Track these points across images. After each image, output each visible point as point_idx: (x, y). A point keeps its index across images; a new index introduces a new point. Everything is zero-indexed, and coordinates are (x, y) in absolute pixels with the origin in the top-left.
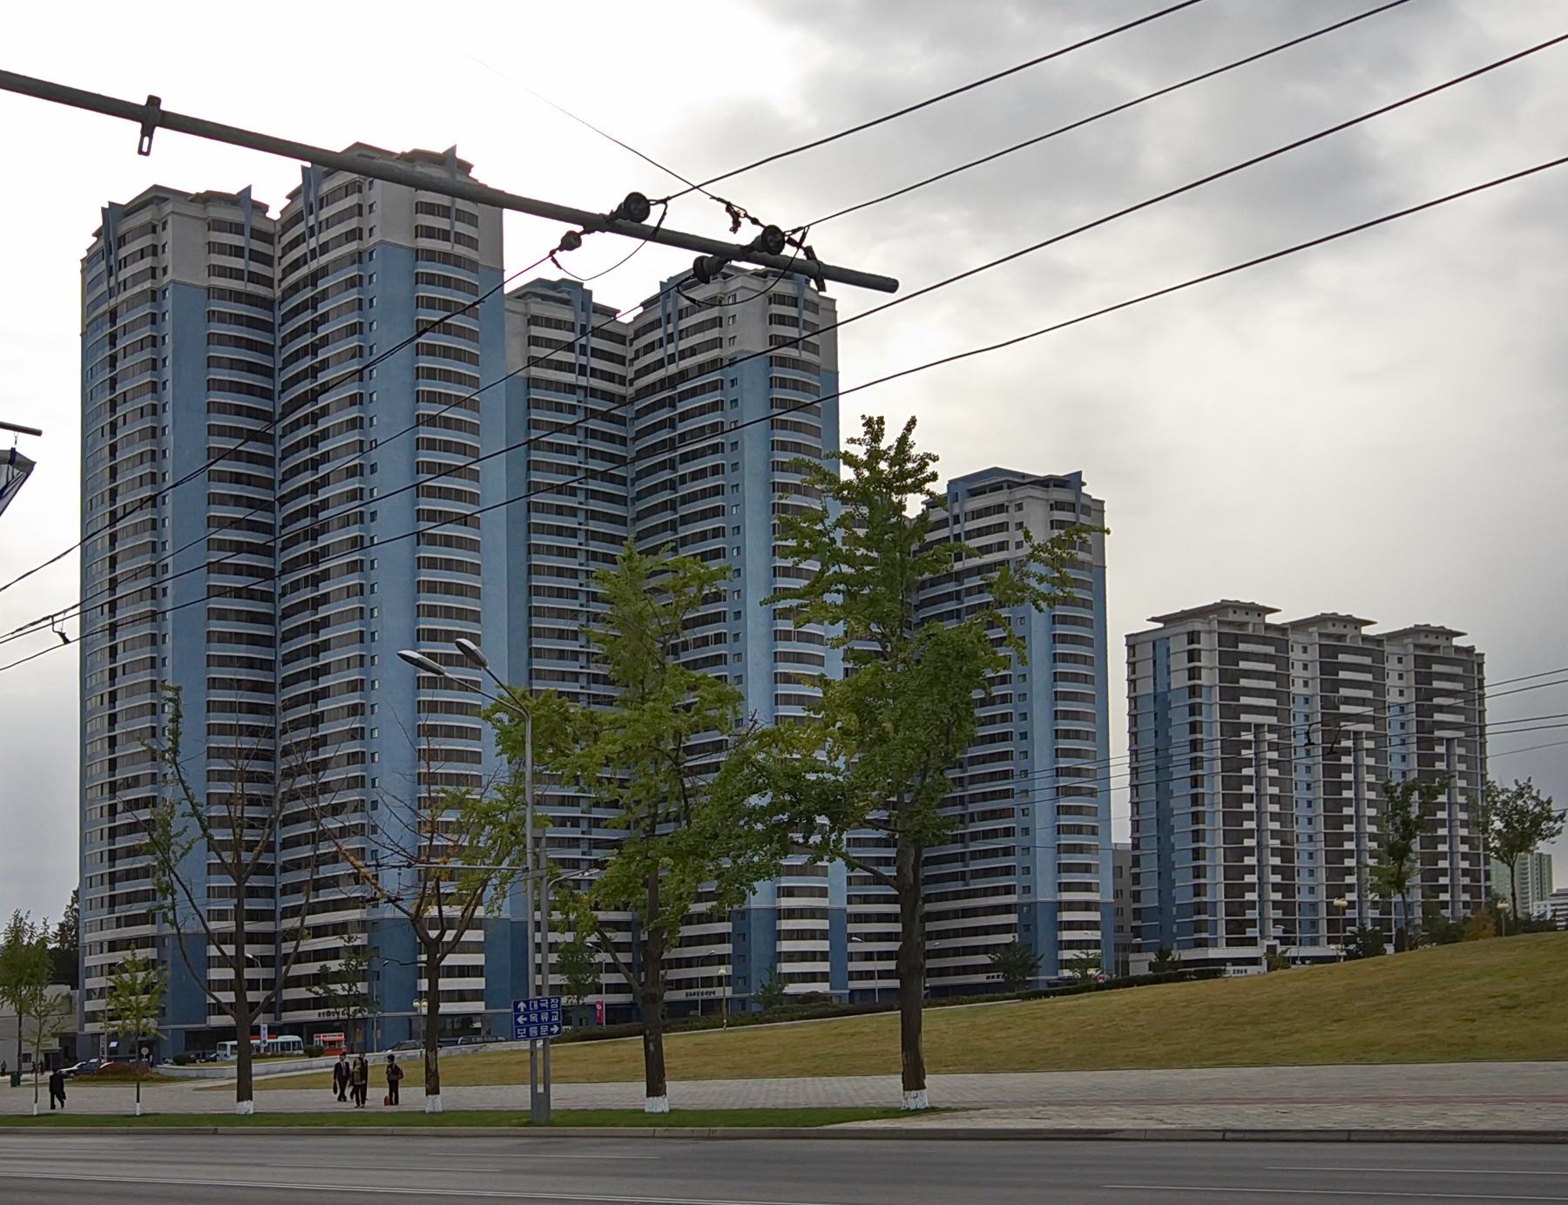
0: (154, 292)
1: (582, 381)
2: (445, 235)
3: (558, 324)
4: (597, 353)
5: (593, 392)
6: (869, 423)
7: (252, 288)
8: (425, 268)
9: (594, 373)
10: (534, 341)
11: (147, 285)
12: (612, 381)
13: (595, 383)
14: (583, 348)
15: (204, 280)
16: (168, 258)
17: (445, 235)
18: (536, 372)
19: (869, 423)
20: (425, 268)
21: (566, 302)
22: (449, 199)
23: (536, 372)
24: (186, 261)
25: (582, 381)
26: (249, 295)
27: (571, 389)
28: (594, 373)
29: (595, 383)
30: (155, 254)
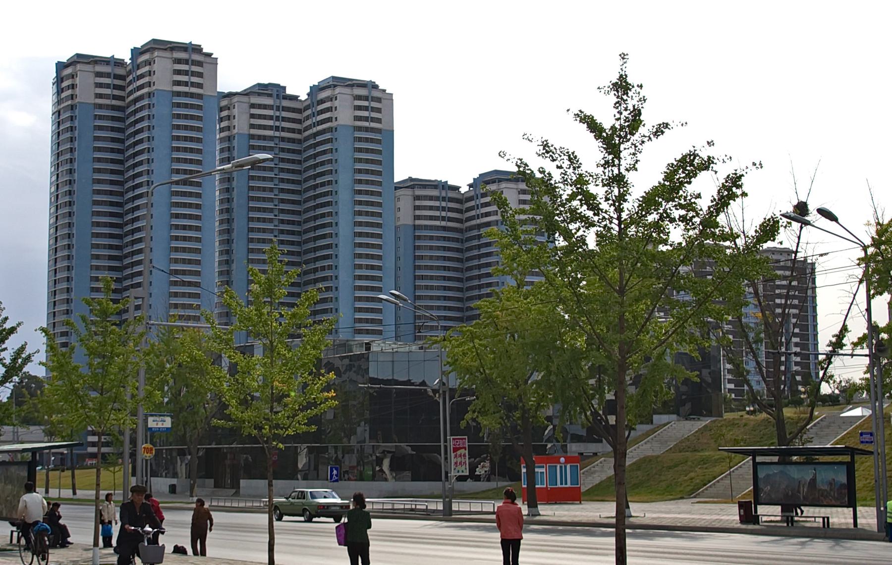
0: (72, 106)
1: (277, 134)
2: (186, 84)
3: (265, 107)
4: (284, 119)
5: (283, 139)
6: (699, 194)
7: (114, 102)
8: (177, 100)
9: (283, 129)
10: (252, 116)
11: (69, 102)
12: (294, 133)
13: (284, 134)
14: (278, 117)
15: (93, 100)
16: (77, 91)
17: (186, 84)
18: (418, 222)
19: (699, 194)
20: (177, 100)
21: (270, 95)
22: (193, 60)
23: (418, 222)
24: (86, 90)
25: (277, 134)
26: (113, 106)
27: (271, 138)
28: (283, 129)
29: (284, 134)
30: (73, 88)
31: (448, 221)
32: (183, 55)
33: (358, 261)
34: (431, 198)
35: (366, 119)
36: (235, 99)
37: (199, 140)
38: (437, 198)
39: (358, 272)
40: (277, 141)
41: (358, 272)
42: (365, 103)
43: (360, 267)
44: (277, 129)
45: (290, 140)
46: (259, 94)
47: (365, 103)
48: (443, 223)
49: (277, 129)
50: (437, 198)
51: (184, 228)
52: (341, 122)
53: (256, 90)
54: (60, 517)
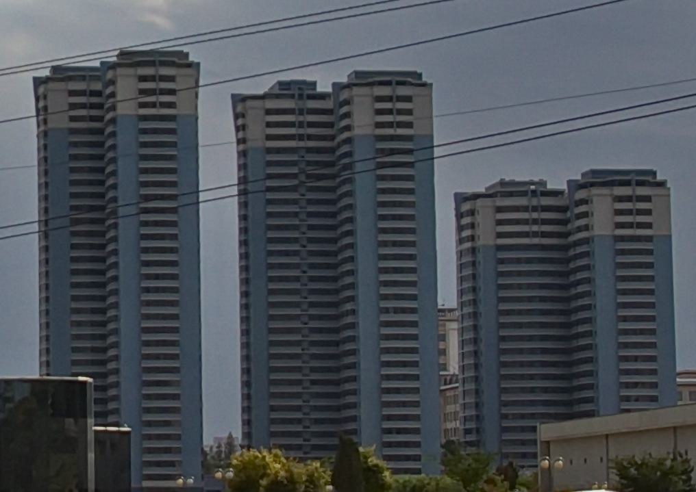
1: (301, 144)
9: (310, 137)
13: (311, 144)
25: (301, 144)
29: (311, 144)
31: (543, 237)
32: (80, 86)
33: (384, 304)
34: (516, 209)
35: (390, 125)
36: (250, 103)
37: (172, 171)
38: (525, 209)
39: (384, 318)
40: (303, 153)
41: (384, 318)
42: (388, 105)
43: (387, 311)
44: (301, 137)
45: (318, 151)
46: (278, 96)
47: (388, 105)
48: (536, 241)
49: (301, 137)
50: (525, 209)
51: (157, 277)
52: (357, 131)
53: (277, 91)
54: (366, 458)
